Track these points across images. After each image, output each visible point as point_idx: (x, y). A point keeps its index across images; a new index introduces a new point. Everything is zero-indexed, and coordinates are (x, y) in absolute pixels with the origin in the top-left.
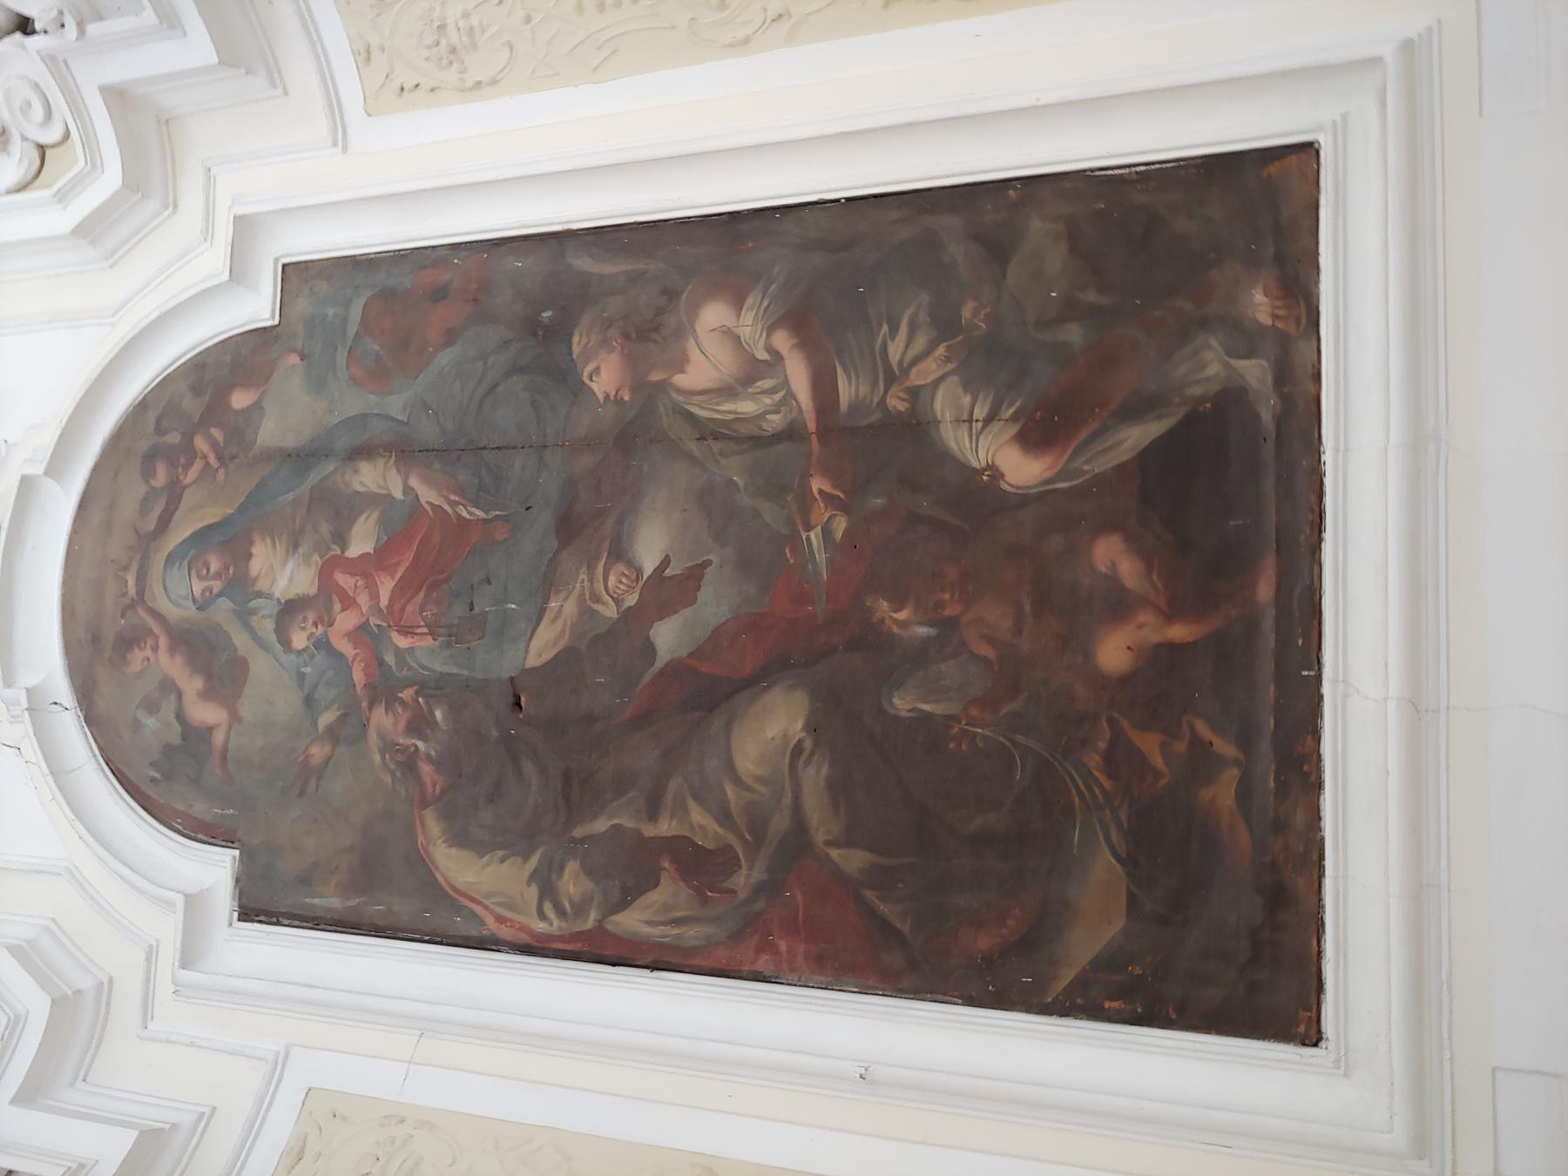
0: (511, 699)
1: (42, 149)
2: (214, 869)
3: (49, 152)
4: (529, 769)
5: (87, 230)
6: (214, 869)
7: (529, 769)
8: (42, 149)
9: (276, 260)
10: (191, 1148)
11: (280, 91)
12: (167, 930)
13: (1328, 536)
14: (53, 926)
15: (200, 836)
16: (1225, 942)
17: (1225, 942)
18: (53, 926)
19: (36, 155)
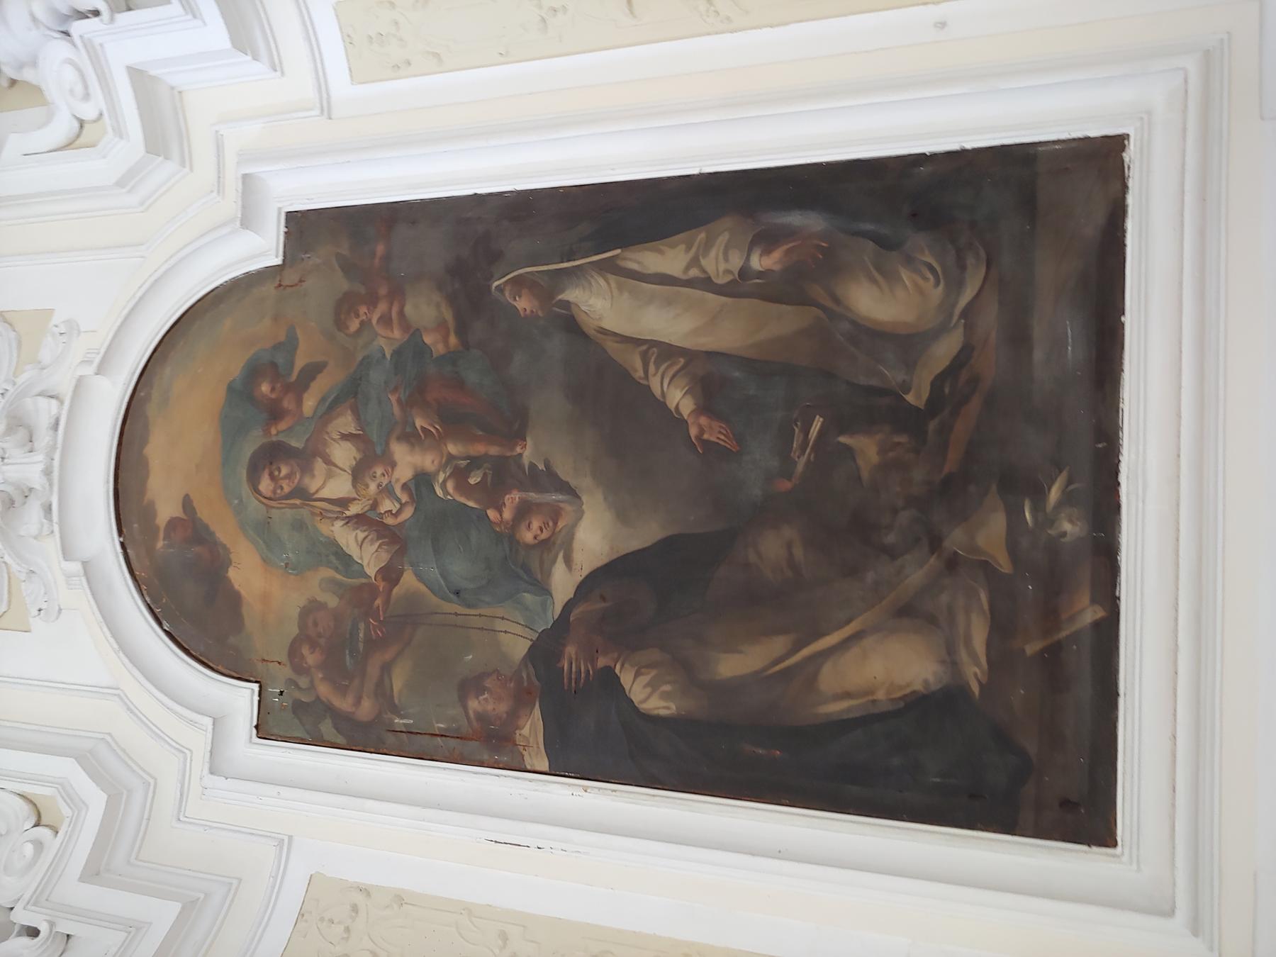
0: (53, 421)
1: (82, 124)
2: (240, 700)
3: (86, 126)
4: (500, 625)
5: (129, 192)
6: (240, 700)
7: (500, 625)
8: (82, 124)
9: (280, 209)
10: (218, 922)
11: (279, 73)
12: (199, 741)
13: (1130, 225)
14: (108, 738)
15: (220, 668)
16: (1021, 751)
17: (1021, 751)
18: (108, 738)
19: (76, 125)
